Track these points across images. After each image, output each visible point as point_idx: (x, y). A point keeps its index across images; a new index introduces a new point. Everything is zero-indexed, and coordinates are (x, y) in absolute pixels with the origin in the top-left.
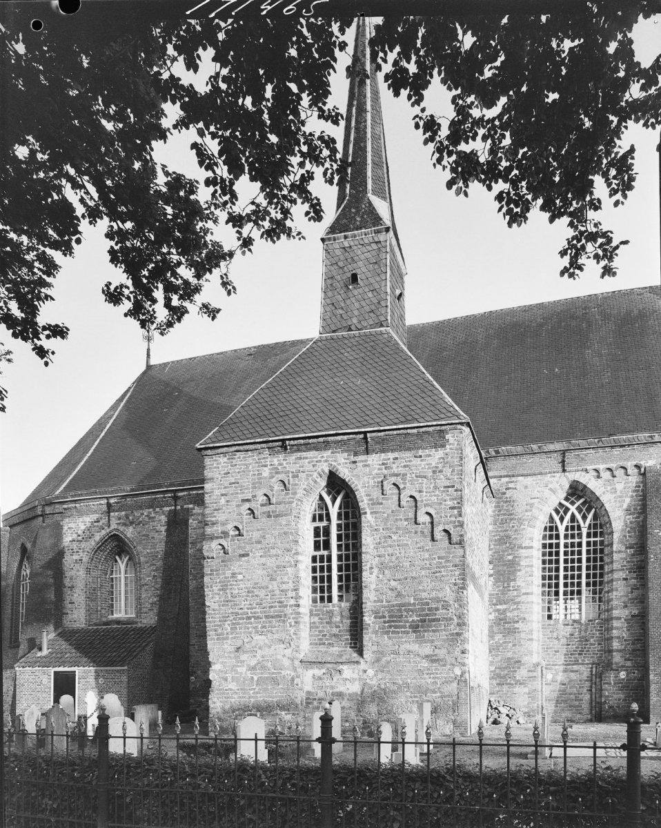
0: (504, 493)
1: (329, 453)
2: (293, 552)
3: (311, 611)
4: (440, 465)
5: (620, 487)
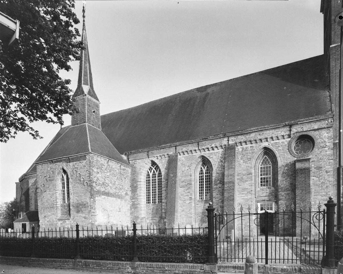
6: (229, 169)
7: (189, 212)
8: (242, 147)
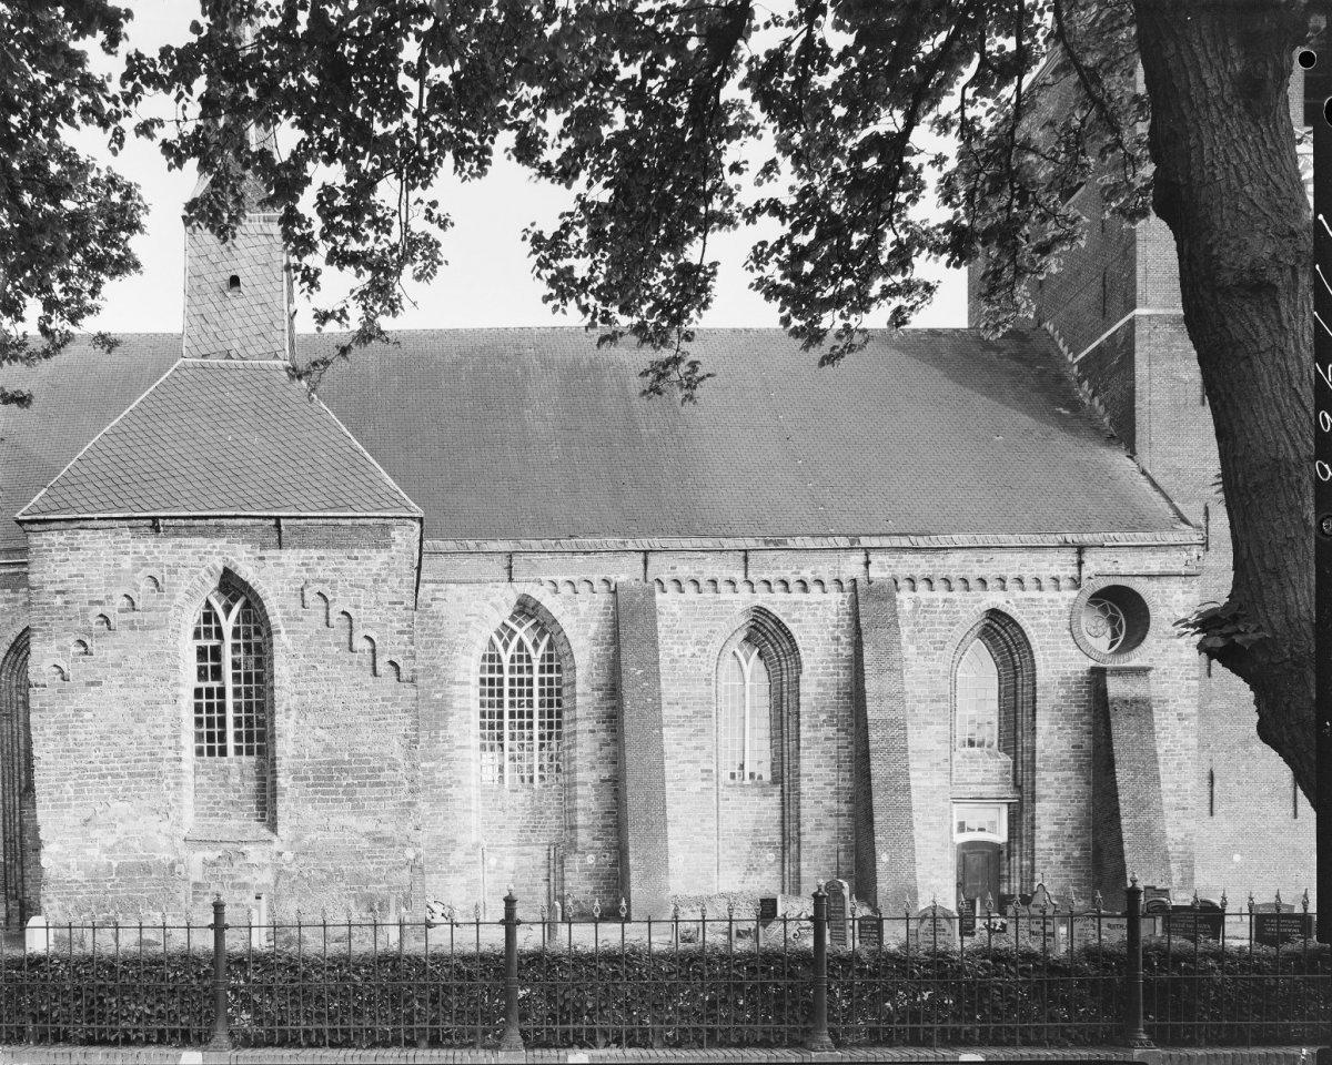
0: (430, 605)
1: (222, 542)
2: (171, 681)
3: (196, 767)
4: (383, 572)
5: (583, 607)
6: (881, 672)
7: (698, 829)
8: (912, 594)
